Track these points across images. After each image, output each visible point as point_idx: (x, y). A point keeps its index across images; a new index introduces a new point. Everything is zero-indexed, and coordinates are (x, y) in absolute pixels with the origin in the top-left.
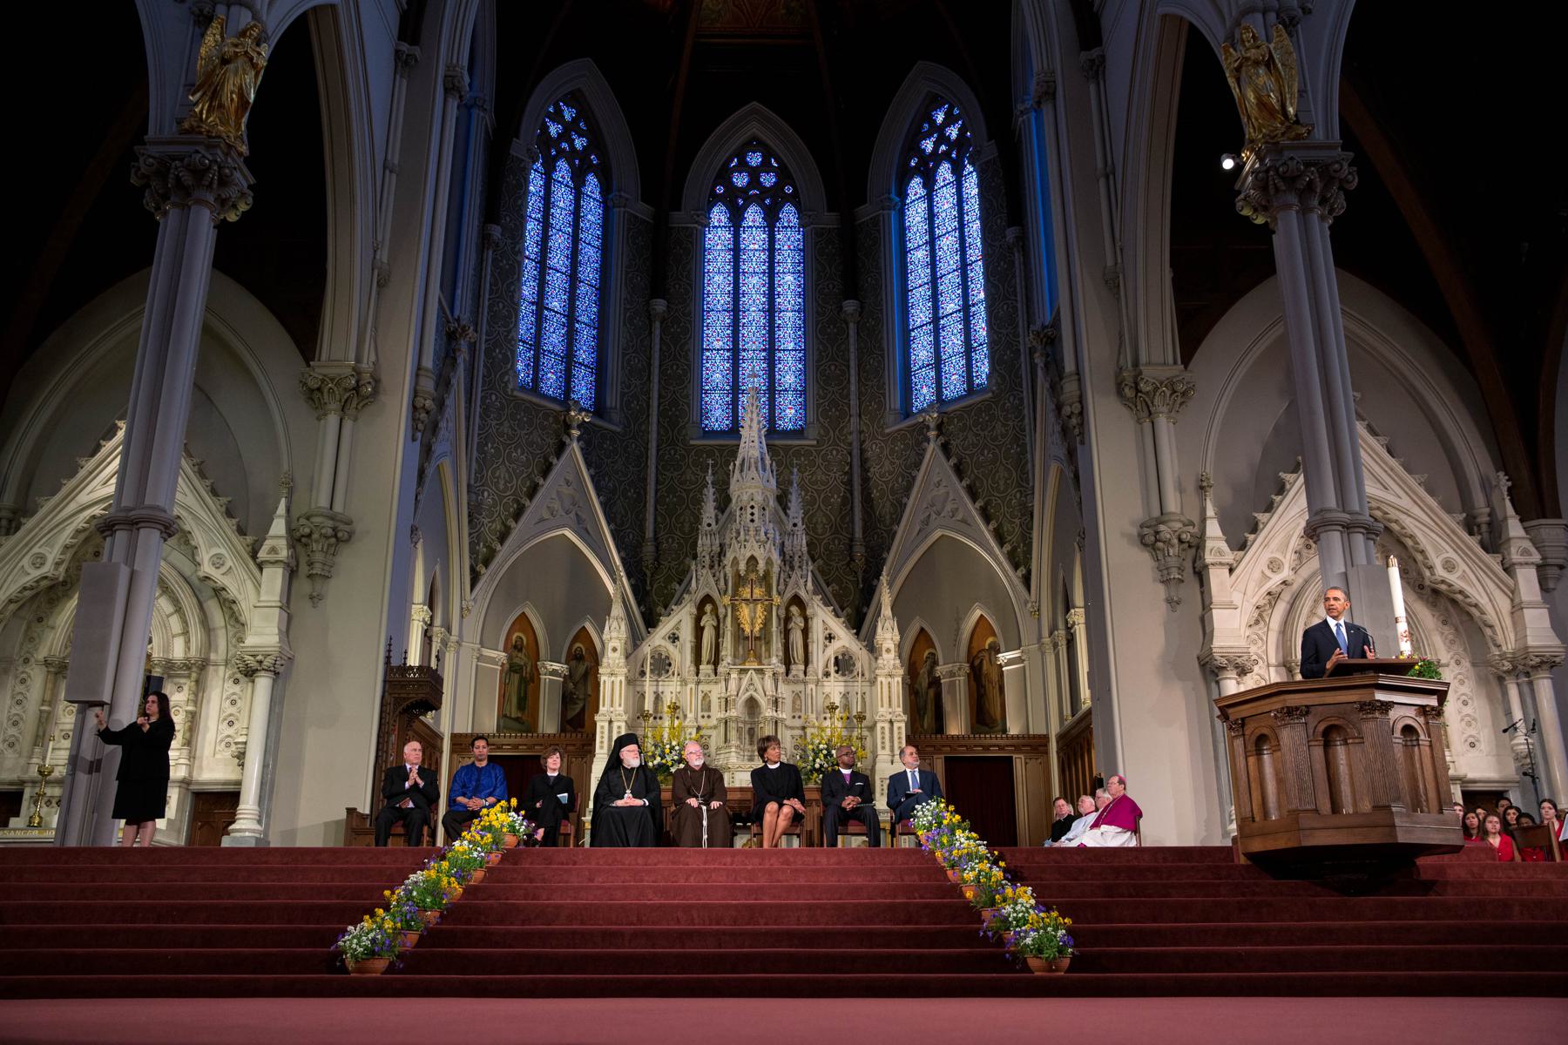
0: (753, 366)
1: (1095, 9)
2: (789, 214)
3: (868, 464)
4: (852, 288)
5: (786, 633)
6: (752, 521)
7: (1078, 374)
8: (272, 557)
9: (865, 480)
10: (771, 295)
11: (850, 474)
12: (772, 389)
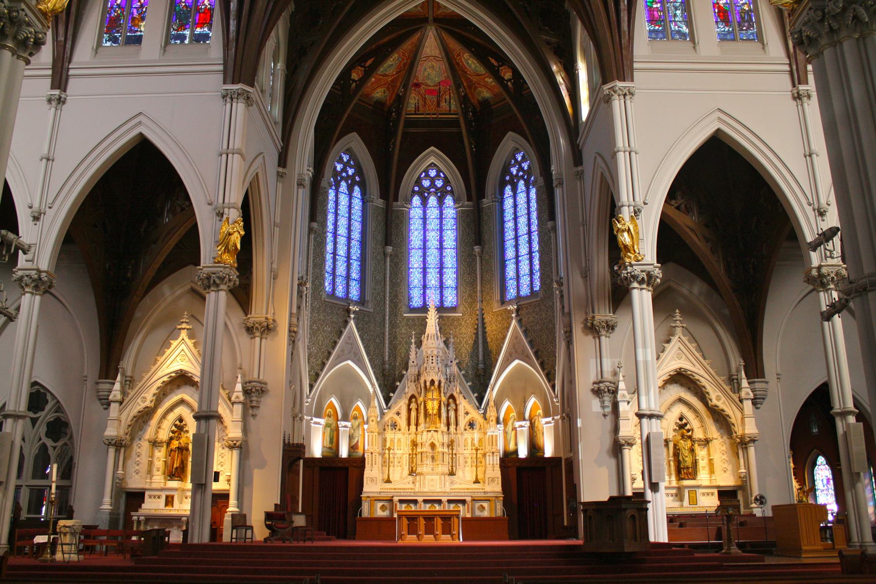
0: (433, 279)
1: (580, 148)
2: (449, 201)
3: (485, 326)
4: (479, 239)
6: (432, 363)
8: (237, 400)
9: (484, 333)
10: (441, 241)
11: (477, 329)
12: (442, 287)
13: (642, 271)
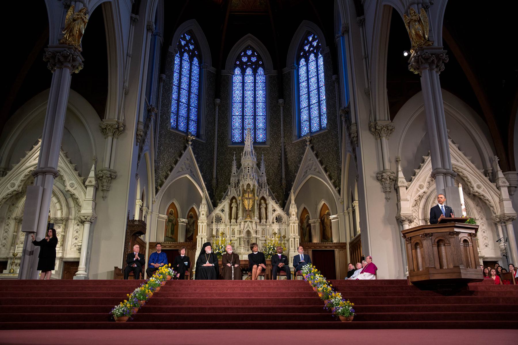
0: (249, 121)
1: (362, 3)
2: (261, 71)
3: (287, 153)
4: (281, 95)
5: (260, 209)
6: (249, 172)
7: (356, 123)
8: (90, 184)
9: (286, 159)
10: (255, 97)
11: (281, 156)
12: (255, 129)
13: (432, 54)
